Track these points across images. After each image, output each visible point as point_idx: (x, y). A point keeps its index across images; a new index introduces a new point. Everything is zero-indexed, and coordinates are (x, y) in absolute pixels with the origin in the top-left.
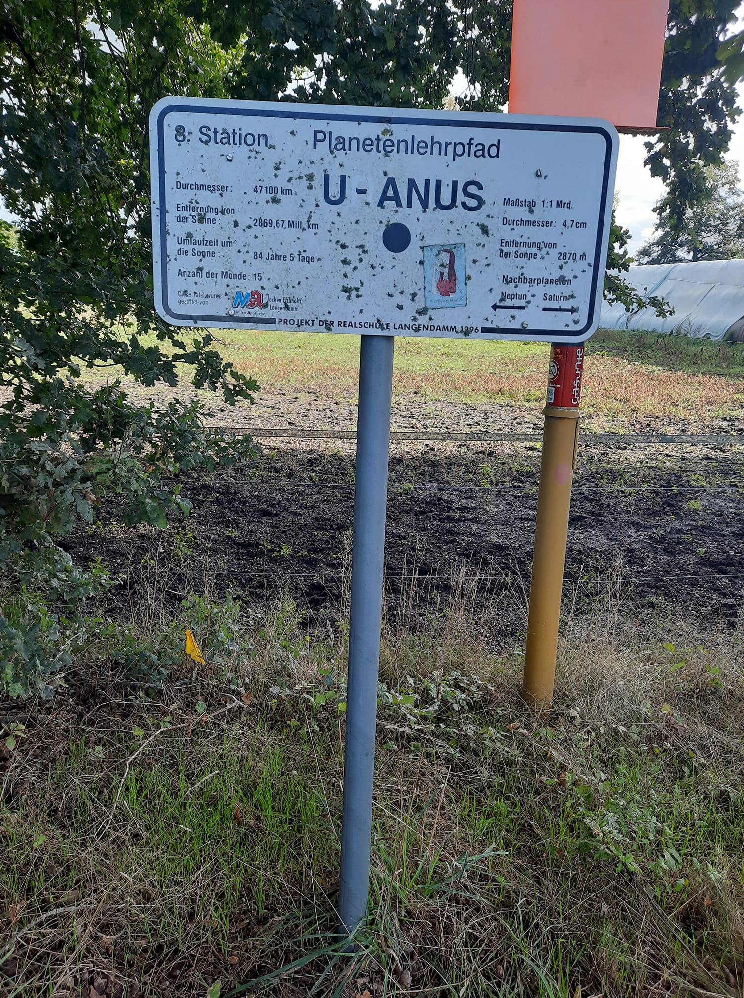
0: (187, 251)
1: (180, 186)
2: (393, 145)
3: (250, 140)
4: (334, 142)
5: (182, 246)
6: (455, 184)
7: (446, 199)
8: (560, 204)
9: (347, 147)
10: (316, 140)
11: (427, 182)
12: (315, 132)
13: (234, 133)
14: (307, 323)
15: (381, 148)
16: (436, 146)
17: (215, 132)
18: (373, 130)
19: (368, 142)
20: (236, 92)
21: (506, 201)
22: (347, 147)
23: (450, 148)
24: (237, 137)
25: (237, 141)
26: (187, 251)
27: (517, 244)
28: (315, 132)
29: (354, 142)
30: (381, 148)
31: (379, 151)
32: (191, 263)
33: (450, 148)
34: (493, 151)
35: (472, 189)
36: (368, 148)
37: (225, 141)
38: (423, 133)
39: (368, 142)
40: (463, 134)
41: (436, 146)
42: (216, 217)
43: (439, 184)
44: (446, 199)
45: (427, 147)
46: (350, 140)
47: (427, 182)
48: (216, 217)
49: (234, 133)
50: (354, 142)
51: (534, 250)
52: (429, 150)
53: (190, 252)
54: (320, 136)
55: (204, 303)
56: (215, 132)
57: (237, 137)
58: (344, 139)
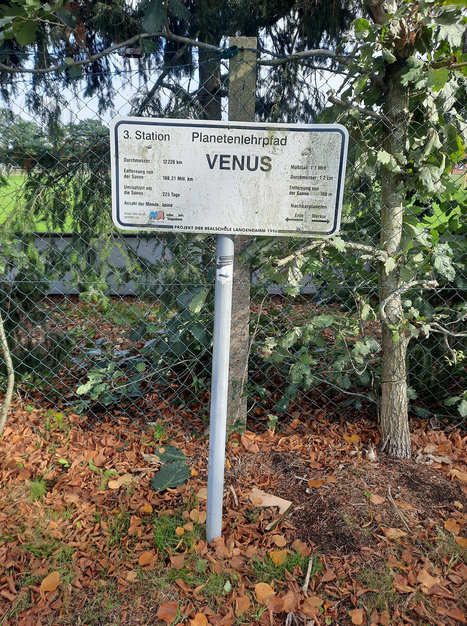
0: (129, 192)
1: (125, 160)
2: (232, 139)
3: (161, 138)
4: (203, 138)
5: (127, 189)
6: (257, 158)
7: (252, 166)
8: (320, 168)
9: (209, 140)
10: (193, 137)
11: (243, 157)
12: (193, 133)
13: (153, 134)
14: (189, 228)
15: (226, 141)
16: (254, 140)
17: (144, 134)
18: (266, 134)
19: (220, 138)
20: (173, 115)
21: (292, 167)
22: (209, 140)
23: (262, 140)
24: (154, 136)
25: (155, 138)
26: (129, 192)
27: (298, 188)
28: (193, 133)
29: (213, 138)
30: (226, 141)
31: (225, 142)
32: (131, 198)
33: (262, 140)
34: (283, 142)
35: (265, 161)
36: (230, 141)
37: (148, 138)
38: (248, 133)
39: (220, 138)
40: (229, 133)
41: (254, 140)
42: (144, 175)
43: (249, 158)
44: (252, 166)
45: (232, 139)
46: (211, 137)
47: (243, 157)
48: (144, 175)
49: (153, 134)
50: (213, 138)
51: (141, 175)
52: (251, 142)
53: (131, 193)
54: (196, 135)
55: (138, 218)
56: (144, 134)
57: (154, 136)
58: (278, 140)
